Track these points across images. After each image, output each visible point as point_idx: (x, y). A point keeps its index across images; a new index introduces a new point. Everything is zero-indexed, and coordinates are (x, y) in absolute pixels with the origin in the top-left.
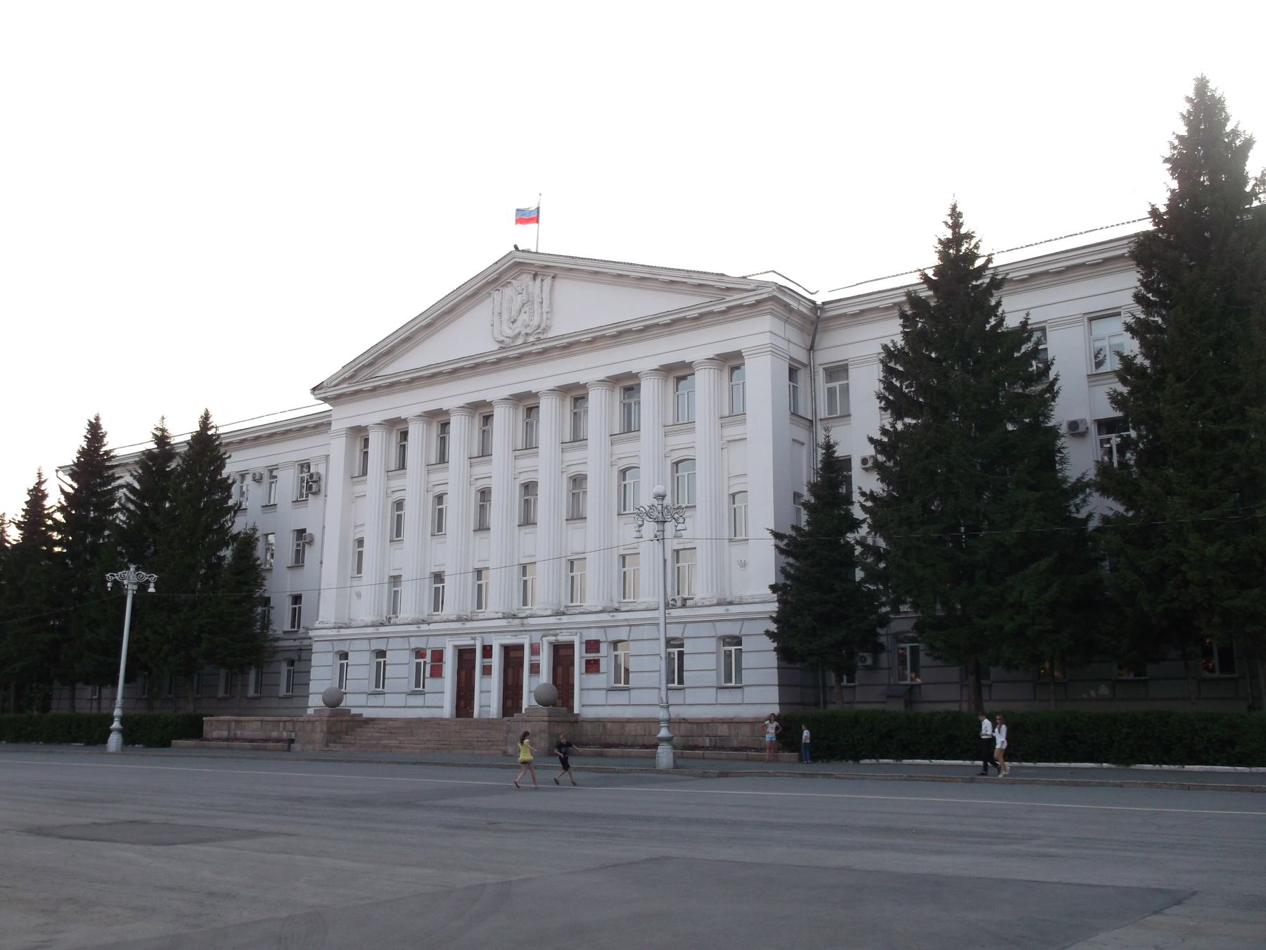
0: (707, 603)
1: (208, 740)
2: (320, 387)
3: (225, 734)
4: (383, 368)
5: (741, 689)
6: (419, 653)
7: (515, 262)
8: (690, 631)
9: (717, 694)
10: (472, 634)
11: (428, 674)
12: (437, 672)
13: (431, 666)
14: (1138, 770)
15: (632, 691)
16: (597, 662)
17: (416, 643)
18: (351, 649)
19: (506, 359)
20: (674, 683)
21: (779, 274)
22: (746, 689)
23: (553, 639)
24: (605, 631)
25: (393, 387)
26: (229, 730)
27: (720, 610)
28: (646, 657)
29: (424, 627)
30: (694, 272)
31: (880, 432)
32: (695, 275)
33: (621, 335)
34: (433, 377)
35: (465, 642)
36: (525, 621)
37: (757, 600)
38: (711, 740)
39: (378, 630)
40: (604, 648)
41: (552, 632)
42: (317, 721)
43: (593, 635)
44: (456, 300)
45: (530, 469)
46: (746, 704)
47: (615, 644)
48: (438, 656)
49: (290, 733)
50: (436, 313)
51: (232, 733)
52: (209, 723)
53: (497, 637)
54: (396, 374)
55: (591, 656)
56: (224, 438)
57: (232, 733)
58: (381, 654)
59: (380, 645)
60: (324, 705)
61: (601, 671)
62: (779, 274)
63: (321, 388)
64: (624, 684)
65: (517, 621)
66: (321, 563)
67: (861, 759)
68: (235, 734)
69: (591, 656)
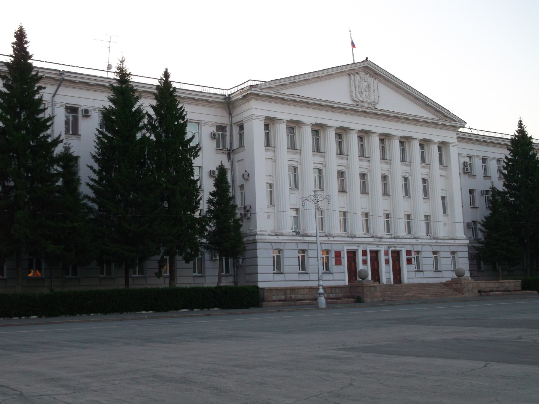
0: (446, 238)
1: (269, 301)
2: (254, 86)
3: (283, 297)
4: (284, 90)
5: (204, 278)
6: (327, 252)
7: (367, 66)
8: (442, 248)
9: (415, 274)
10: (359, 244)
11: (334, 263)
12: (338, 262)
13: (336, 259)
14: (182, 312)
15: (425, 272)
16: (411, 259)
17: (325, 247)
18: (285, 248)
19: (355, 111)
20: (167, 273)
21: (62, 64)
22: (443, 272)
23: (393, 249)
24: (413, 246)
25: (283, 100)
26: (286, 295)
27: (452, 241)
28: (428, 258)
29: (331, 239)
30: (441, 106)
31: (218, 167)
32: (441, 108)
33: (397, 118)
34: (307, 104)
35: (352, 248)
36: (381, 240)
37: (461, 239)
38: (504, 289)
39: (455, 242)
40: (413, 253)
41: (394, 245)
42: (378, 286)
43: (409, 248)
44: (394, 81)
45: (384, 169)
46: (417, 278)
47: (418, 252)
48: (338, 254)
49: (329, 294)
50: (406, 89)
51: (288, 296)
52: (269, 291)
53: (369, 246)
54: (287, 95)
55: (409, 257)
56: (67, 76)
57: (288, 296)
58: (303, 251)
59: (436, 249)
60: (456, 276)
61: (413, 264)
62: (91, 69)
63: (255, 87)
64: (225, 273)
65: (378, 240)
66: (462, 207)
67: (211, 308)
68: (291, 297)
69: (409, 257)
